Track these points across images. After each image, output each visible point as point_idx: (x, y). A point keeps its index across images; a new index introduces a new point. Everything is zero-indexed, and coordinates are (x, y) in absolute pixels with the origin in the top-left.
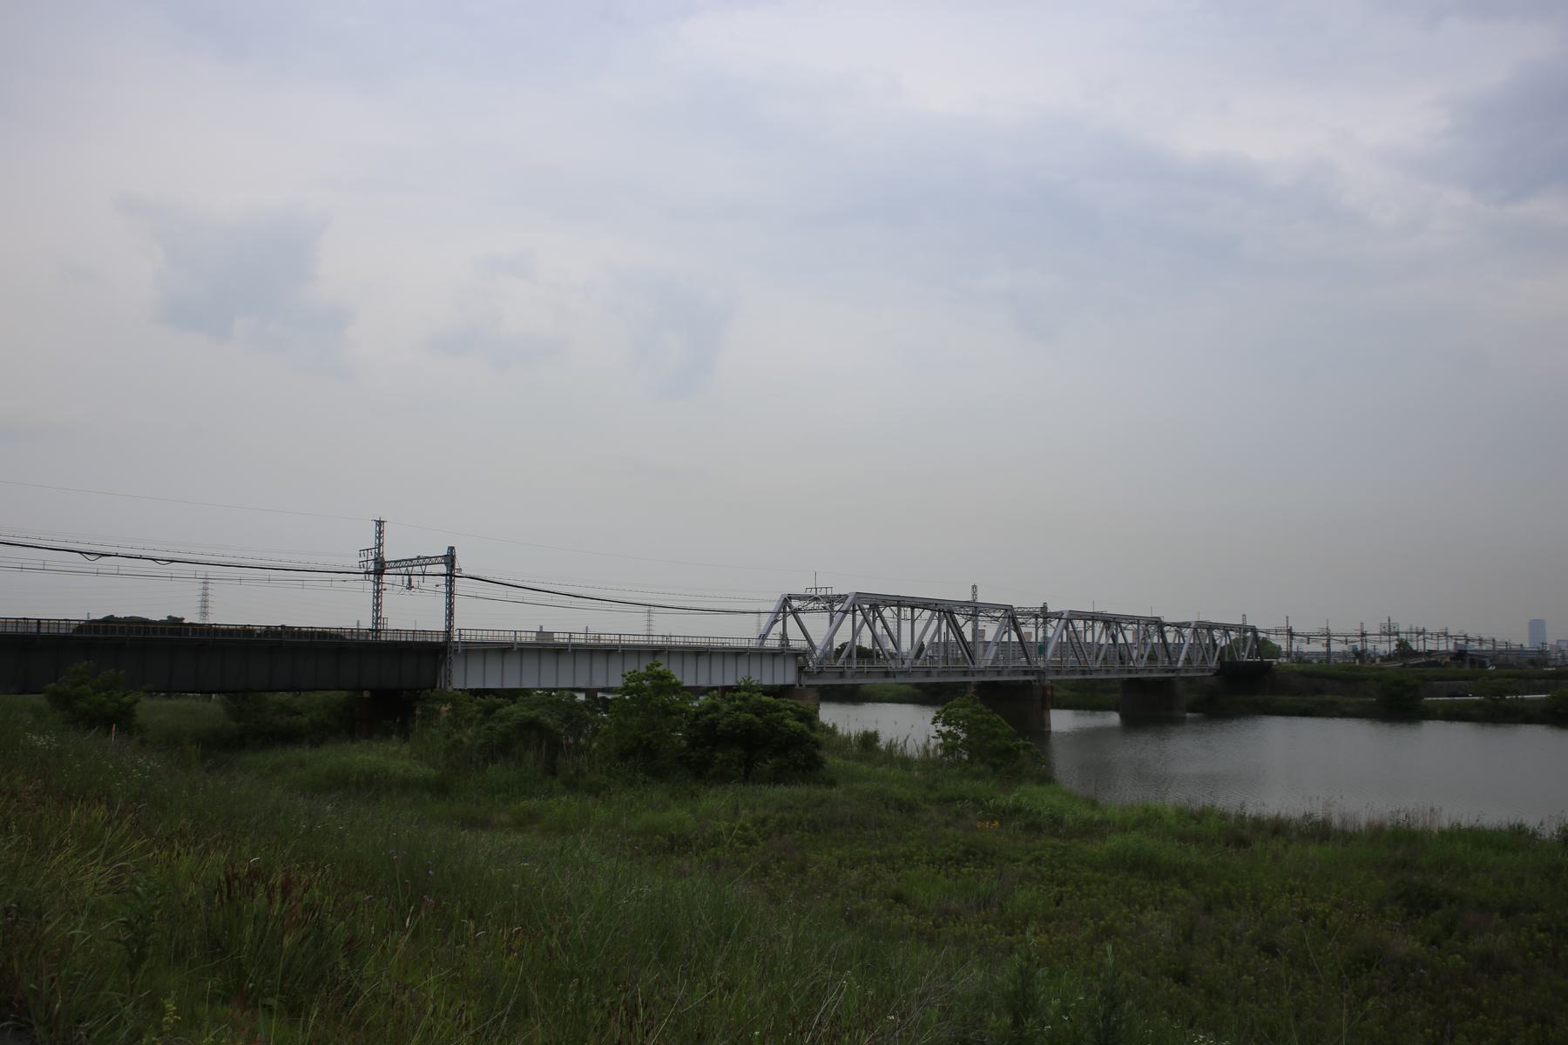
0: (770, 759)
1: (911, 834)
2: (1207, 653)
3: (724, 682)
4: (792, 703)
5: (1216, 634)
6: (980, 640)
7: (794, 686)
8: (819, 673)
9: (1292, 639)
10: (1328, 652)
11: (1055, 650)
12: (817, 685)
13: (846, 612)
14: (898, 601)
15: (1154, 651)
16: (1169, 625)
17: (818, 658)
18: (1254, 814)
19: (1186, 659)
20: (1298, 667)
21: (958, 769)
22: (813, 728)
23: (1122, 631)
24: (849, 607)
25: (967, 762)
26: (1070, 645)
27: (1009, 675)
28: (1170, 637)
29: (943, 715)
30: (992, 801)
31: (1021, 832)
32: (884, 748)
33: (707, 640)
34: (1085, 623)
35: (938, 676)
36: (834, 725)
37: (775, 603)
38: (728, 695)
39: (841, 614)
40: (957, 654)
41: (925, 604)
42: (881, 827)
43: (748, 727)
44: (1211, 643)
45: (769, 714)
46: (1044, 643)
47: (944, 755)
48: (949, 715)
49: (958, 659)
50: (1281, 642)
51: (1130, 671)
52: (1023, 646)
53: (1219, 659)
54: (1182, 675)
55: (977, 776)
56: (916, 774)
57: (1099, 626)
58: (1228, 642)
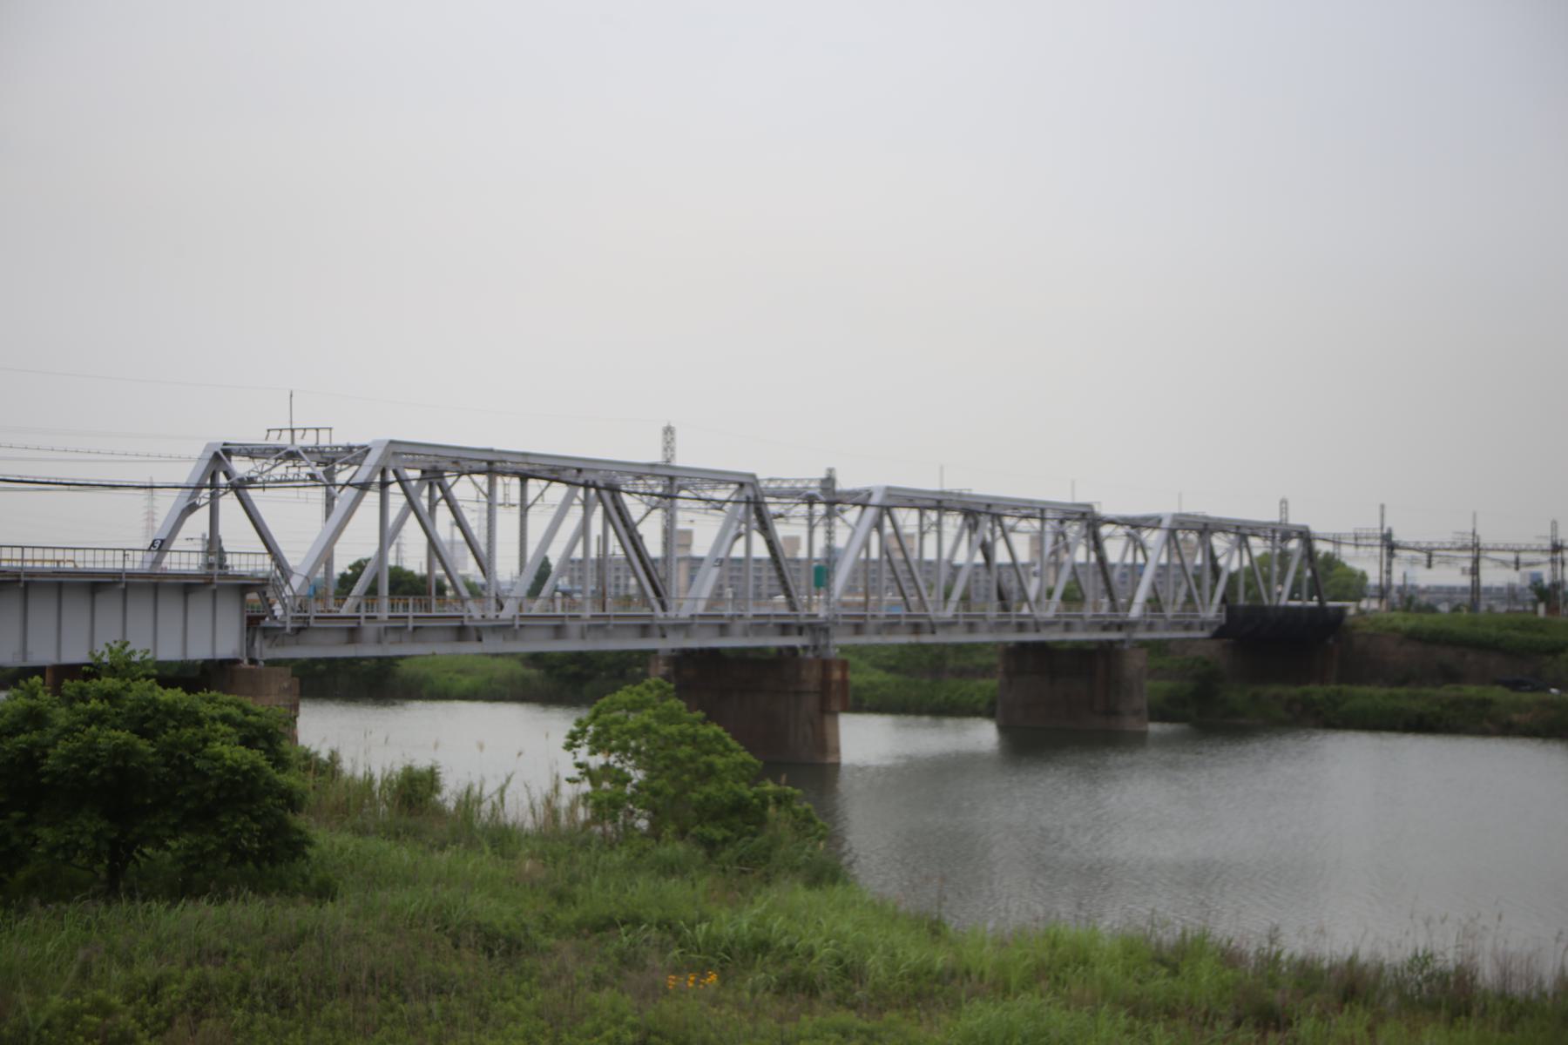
0: (174, 837)
1: (512, 1007)
2: (1199, 586)
3: (59, 655)
4: (230, 703)
5: (1220, 543)
6: (679, 553)
7: (236, 662)
8: (298, 630)
9: (1391, 555)
10: (1475, 589)
11: (853, 576)
12: (293, 660)
13: (364, 487)
14: (490, 463)
15: (1077, 581)
16: (1112, 522)
17: (295, 596)
18: (1300, 953)
19: (1149, 601)
20: (1405, 620)
21: (625, 851)
22: (280, 762)
23: (1005, 536)
24: (372, 474)
25: (644, 836)
26: (886, 567)
27: (746, 634)
28: (1115, 550)
29: (591, 728)
30: (704, 926)
31: (767, 996)
32: (451, 805)
33: (17, 554)
34: (921, 515)
35: (583, 637)
36: (334, 757)
37: (192, 465)
38: (70, 686)
39: (353, 492)
40: (627, 586)
41: (554, 471)
42: (441, 992)
43: (119, 763)
44: (1208, 564)
45: (172, 732)
46: (827, 561)
47: (594, 820)
48: (605, 727)
49: (628, 598)
50: (1366, 563)
51: (1021, 627)
52: (779, 569)
53: (1224, 600)
54: (1142, 635)
55: (670, 869)
56: (528, 865)
57: (953, 522)
58: (1246, 562)
